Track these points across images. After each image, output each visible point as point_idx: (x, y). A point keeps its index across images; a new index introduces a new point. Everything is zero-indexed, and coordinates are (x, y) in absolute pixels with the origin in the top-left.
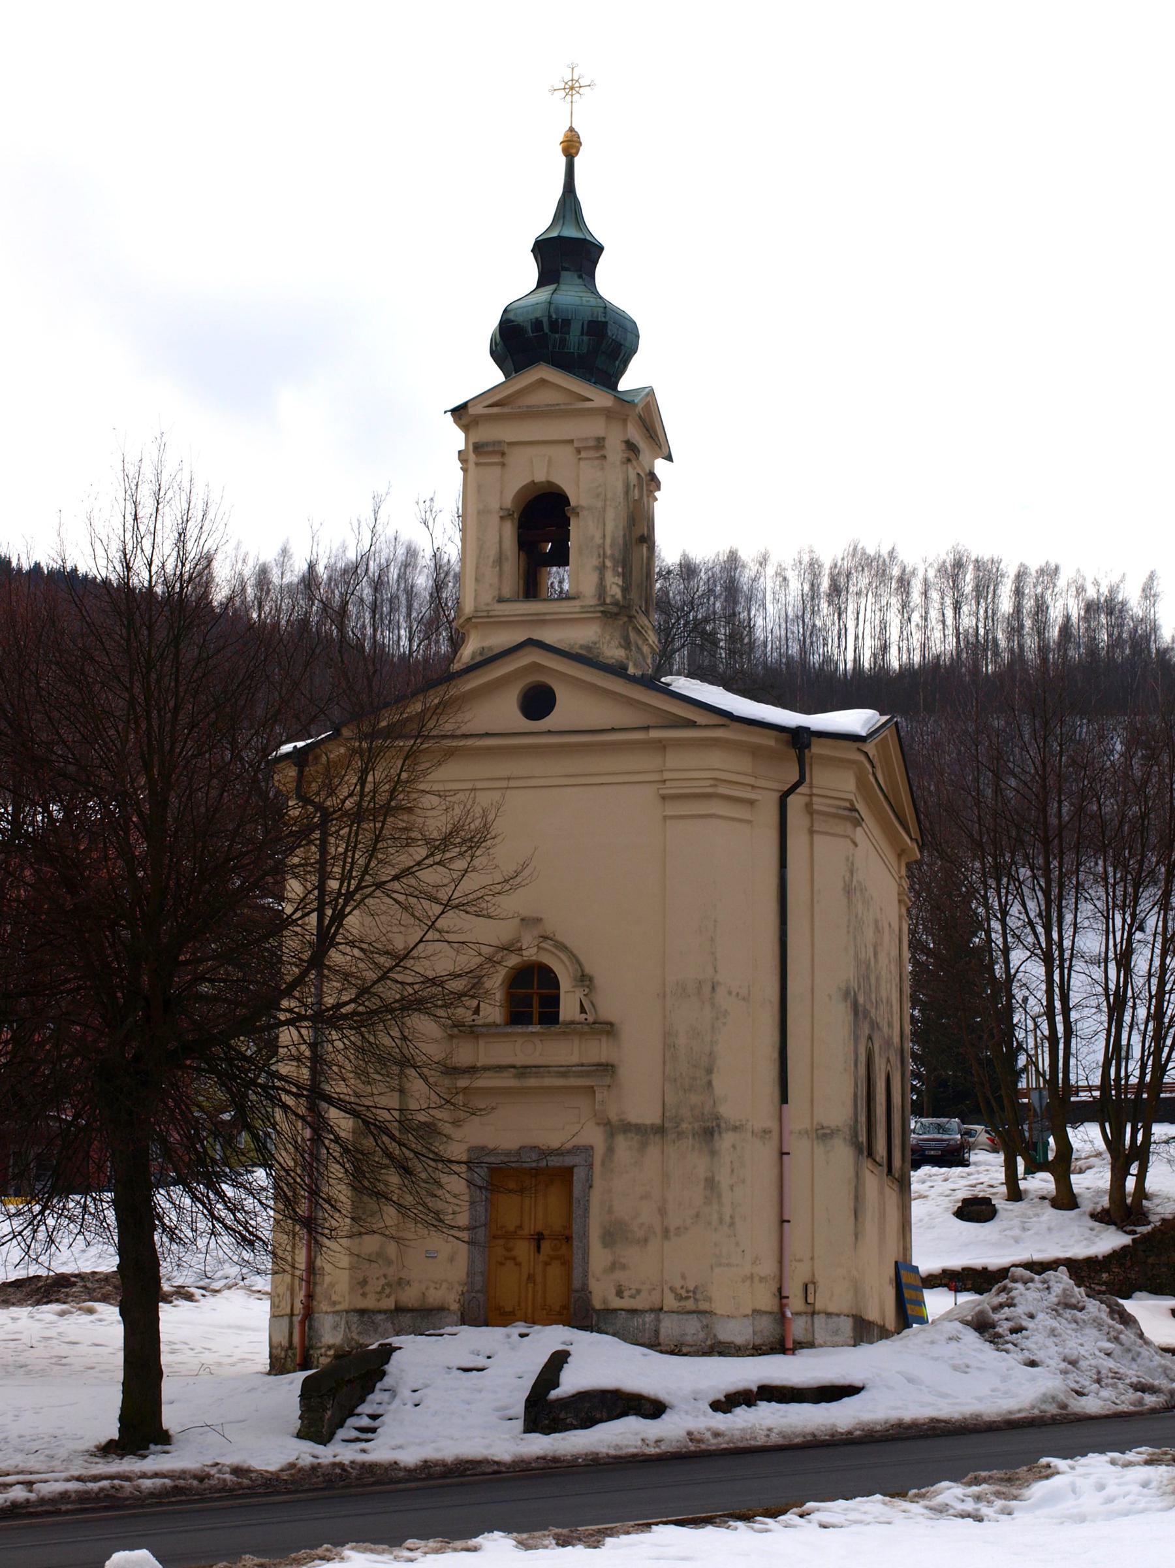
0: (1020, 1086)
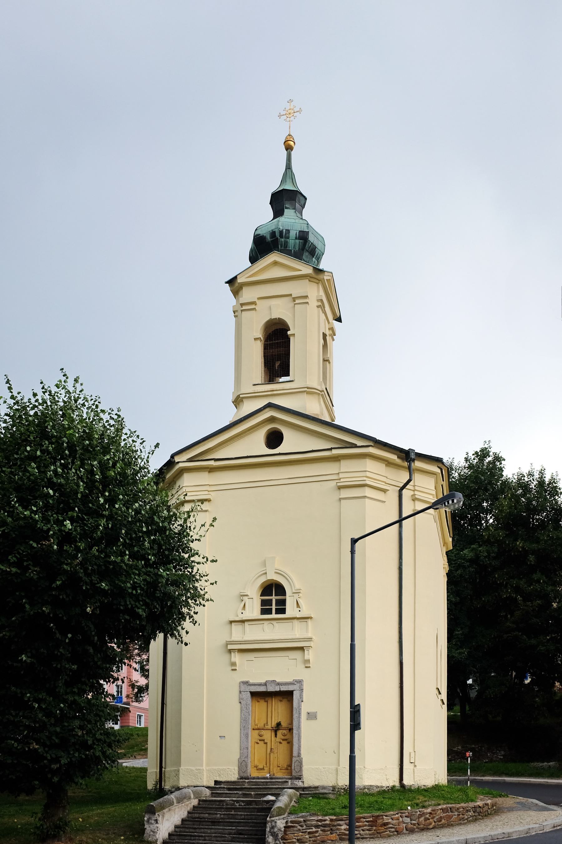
0: (64, 549)
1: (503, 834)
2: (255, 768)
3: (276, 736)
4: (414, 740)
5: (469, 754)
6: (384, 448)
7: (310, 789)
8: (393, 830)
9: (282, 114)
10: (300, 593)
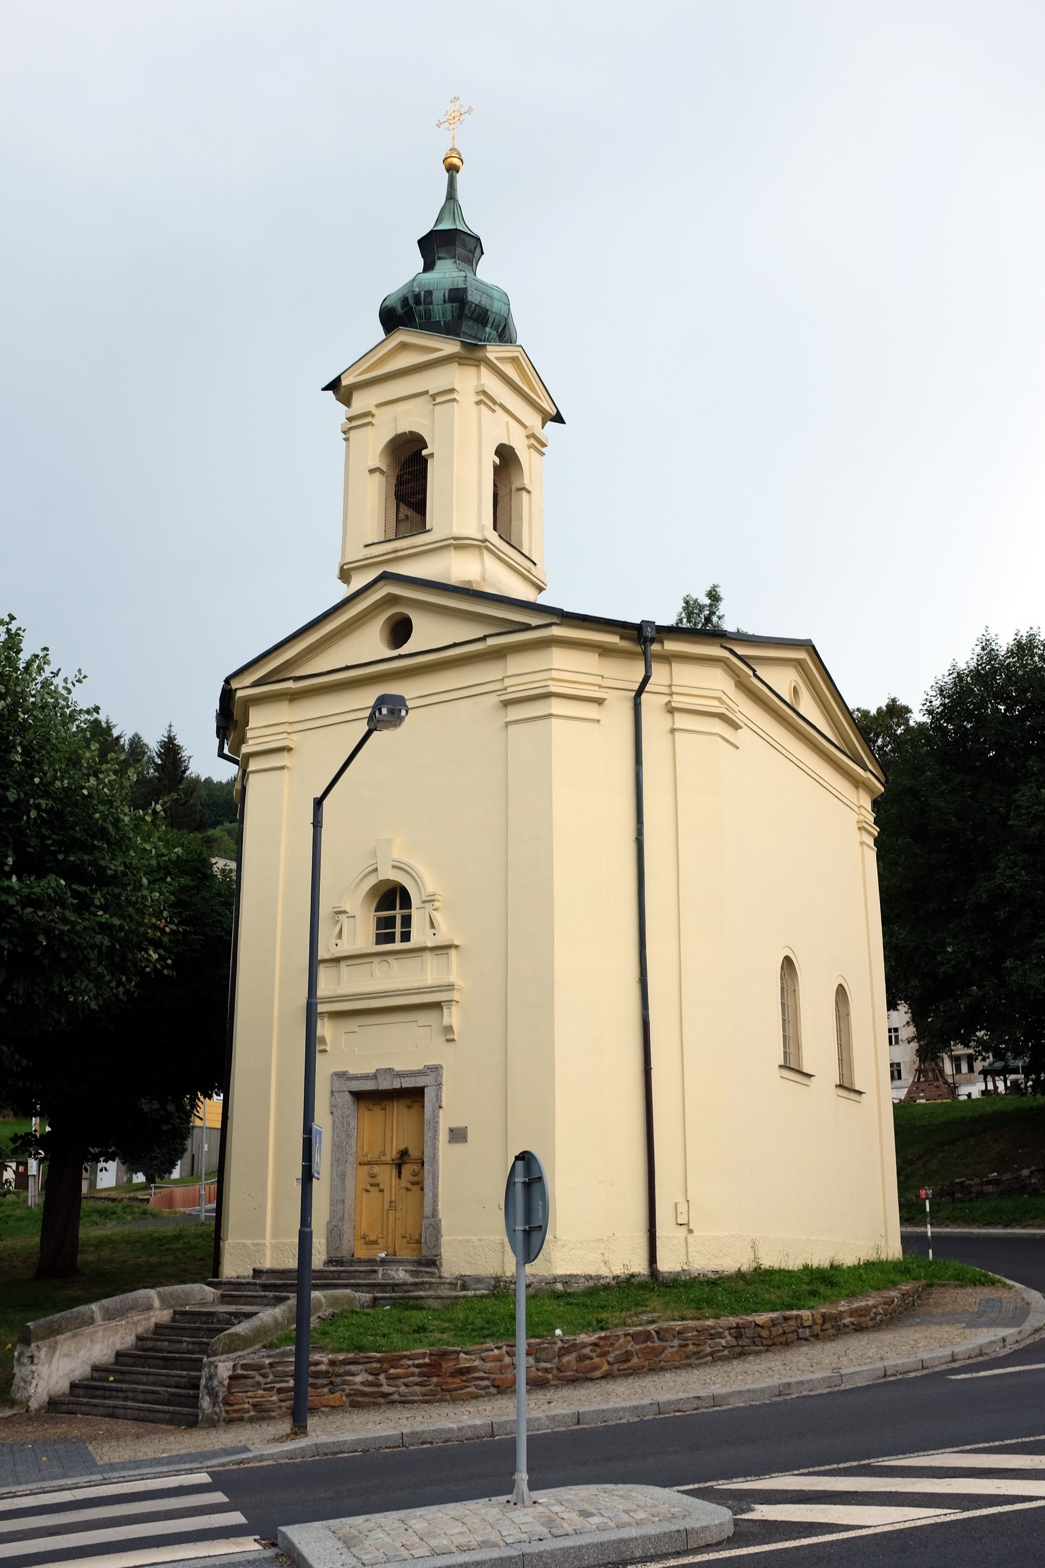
1: (696, 1401)
2: (363, 1241)
3: (400, 1177)
4: (686, 1176)
5: (926, 1194)
6: (585, 624)
7: (405, 1287)
8: (486, 1383)
9: (442, 121)
10: (433, 901)
